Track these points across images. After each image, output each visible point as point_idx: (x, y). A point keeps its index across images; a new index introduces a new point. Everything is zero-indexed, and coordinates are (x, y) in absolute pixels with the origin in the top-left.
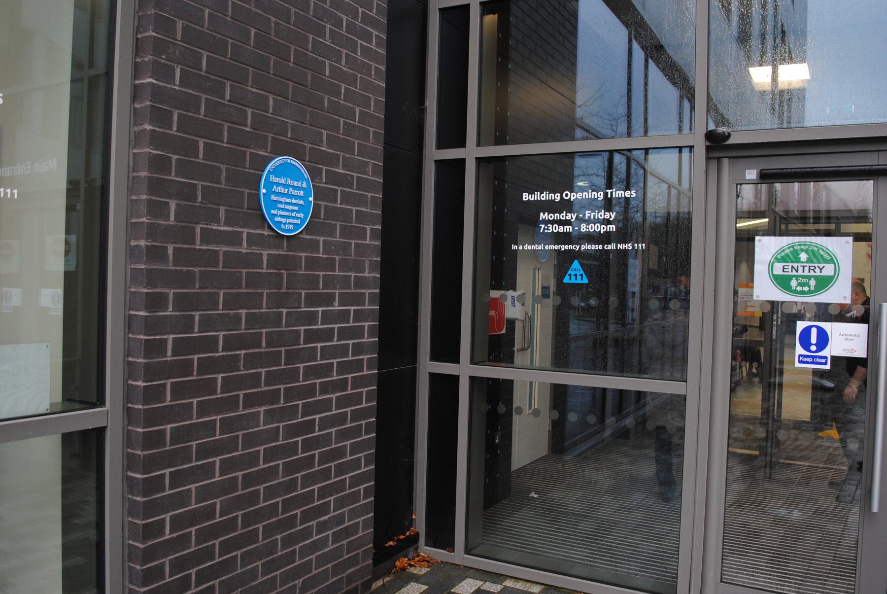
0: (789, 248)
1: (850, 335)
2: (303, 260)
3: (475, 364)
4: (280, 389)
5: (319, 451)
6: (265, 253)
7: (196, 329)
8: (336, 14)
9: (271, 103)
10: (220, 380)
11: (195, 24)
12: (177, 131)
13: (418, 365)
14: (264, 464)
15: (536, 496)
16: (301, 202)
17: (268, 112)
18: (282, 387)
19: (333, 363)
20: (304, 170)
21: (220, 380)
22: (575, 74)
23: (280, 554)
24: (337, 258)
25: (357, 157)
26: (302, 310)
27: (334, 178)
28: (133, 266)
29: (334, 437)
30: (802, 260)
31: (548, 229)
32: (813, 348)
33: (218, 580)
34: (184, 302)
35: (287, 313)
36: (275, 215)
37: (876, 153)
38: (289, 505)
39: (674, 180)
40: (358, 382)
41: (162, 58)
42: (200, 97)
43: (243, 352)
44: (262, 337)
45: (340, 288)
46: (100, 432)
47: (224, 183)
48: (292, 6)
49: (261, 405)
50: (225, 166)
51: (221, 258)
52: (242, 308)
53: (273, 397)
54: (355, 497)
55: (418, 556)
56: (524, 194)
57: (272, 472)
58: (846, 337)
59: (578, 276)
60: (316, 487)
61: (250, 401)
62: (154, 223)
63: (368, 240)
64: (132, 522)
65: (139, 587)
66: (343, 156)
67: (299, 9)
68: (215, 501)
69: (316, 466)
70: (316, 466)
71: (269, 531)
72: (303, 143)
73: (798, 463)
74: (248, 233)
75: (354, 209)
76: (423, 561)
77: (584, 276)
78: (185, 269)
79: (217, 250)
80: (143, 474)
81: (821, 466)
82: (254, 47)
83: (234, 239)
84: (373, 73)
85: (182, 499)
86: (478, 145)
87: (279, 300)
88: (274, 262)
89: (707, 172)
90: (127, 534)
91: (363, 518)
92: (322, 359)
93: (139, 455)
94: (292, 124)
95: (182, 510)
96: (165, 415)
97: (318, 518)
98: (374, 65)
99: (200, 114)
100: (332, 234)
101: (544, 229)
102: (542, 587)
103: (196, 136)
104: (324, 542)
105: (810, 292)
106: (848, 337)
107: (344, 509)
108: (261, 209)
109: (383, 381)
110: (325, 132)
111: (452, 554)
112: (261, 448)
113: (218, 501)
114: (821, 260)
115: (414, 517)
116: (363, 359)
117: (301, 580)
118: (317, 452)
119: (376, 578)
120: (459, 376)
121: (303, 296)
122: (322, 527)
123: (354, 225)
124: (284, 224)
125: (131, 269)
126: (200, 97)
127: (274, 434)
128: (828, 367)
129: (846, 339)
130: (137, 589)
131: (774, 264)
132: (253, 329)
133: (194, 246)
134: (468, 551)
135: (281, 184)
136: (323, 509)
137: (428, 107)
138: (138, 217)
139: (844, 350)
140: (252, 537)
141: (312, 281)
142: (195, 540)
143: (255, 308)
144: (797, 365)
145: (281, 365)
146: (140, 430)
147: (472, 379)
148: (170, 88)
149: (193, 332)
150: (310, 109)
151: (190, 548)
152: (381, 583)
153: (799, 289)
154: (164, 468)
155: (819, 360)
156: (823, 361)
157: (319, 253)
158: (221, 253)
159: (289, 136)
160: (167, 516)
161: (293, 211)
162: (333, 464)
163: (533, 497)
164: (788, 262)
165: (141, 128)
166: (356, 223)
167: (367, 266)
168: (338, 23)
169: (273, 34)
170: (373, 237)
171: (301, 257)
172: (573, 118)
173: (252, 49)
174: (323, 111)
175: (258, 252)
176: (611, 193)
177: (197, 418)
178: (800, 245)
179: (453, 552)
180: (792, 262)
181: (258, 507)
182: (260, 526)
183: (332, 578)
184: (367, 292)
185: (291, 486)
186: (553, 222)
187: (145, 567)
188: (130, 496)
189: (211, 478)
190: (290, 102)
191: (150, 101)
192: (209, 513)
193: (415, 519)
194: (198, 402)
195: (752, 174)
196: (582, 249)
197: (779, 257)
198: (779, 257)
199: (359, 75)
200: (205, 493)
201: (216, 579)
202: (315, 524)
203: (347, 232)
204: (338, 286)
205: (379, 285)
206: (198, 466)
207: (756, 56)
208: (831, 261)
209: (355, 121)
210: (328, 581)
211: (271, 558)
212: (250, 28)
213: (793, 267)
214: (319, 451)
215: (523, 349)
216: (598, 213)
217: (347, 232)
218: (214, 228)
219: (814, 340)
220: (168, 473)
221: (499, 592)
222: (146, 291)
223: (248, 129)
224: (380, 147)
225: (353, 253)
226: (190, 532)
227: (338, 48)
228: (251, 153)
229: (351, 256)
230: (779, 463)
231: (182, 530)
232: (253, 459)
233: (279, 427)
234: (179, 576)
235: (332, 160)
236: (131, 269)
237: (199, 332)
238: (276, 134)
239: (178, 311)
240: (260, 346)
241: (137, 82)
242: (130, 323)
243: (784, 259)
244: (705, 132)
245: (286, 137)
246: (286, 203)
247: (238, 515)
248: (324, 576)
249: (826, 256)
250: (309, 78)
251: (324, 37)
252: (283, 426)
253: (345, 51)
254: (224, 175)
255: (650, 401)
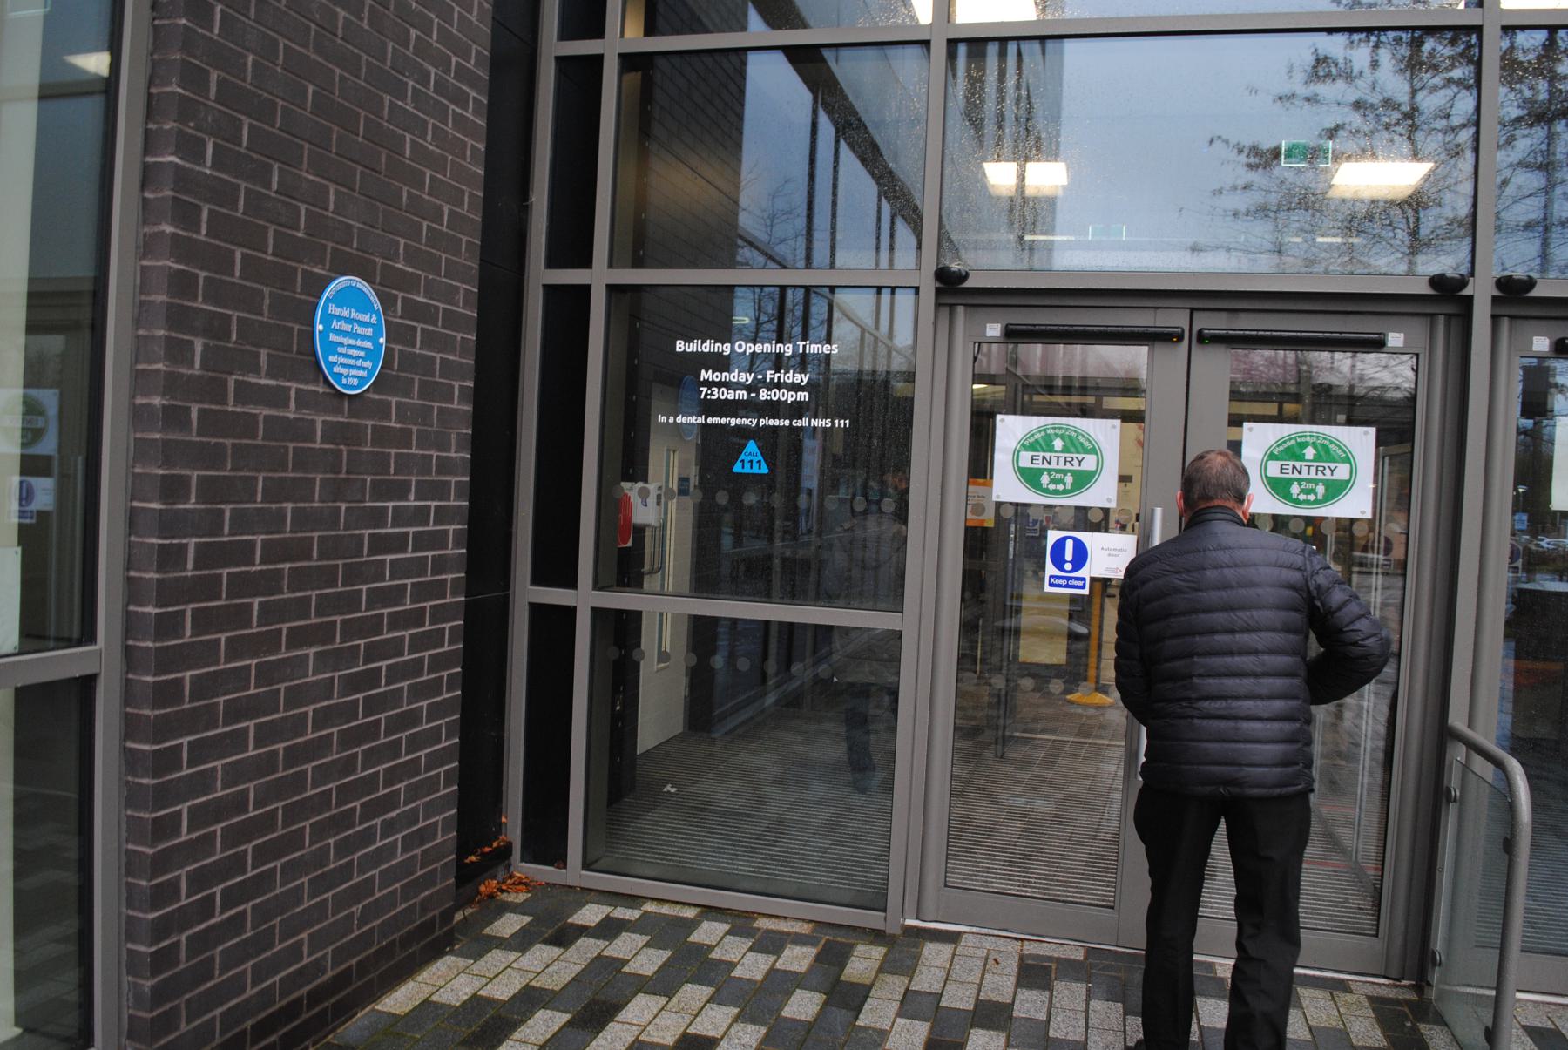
0: (1040, 432)
1: (1115, 550)
2: (369, 432)
3: (600, 589)
4: (336, 621)
5: (386, 714)
6: (319, 420)
7: (227, 529)
8: (422, 65)
9: (332, 198)
10: (256, 607)
11: (234, 76)
12: (206, 235)
13: (511, 591)
14: (312, 732)
15: (673, 790)
16: (369, 345)
17: (327, 210)
18: (338, 618)
19: (406, 585)
20: (373, 297)
21: (256, 607)
22: (740, 161)
23: (332, 866)
24: (415, 429)
25: (444, 280)
26: (367, 504)
27: (412, 310)
28: (138, 435)
29: (405, 695)
30: (1056, 448)
31: (711, 394)
32: (1068, 566)
33: (251, 904)
34: (213, 491)
35: (347, 508)
36: (335, 364)
37: (1152, 311)
38: (346, 793)
39: (869, 322)
40: (439, 614)
41: (190, 127)
42: (238, 186)
43: (287, 566)
44: (312, 545)
45: (417, 475)
46: (87, 684)
47: (266, 313)
48: (364, 52)
49: (311, 645)
50: (269, 289)
51: (261, 426)
52: (287, 500)
53: (325, 633)
54: (432, 784)
55: (511, 877)
56: (678, 342)
57: (322, 745)
58: (1108, 552)
59: (754, 462)
60: (381, 768)
61: (299, 638)
62: (174, 372)
63: (456, 402)
64: (133, 817)
65: (146, 912)
66: (426, 278)
67: (373, 57)
68: (247, 785)
69: (382, 736)
70: (382, 736)
71: (320, 831)
72: (372, 257)
73: (1039, 736)
74: (297, 389)
75: (438, 356)
76: (520, 883)
77: (763, 463)
78: (213, 441)
79: (255, 415)
80: (154, 743)
81: (1072, 739)
82: (311, 113)
83: (277, 398)
84: (468, 153)
85: (203, 783)
86: (611, 266)
87: (336, 490)
88: (332, 432)
89: (935, 324)
90: (124, 835)
91: (443, 816)
92: (392, 578)
93: (148, 717)
94: (358, 228)
95: (204, 799)
96: (184, 658)
97: (384, 814)
98: (470, 142)
99: (237, 210)
100: (408, 394)
101: (706, 394)
102: (698, 909)
103: (232, 243)
104: (390, 851)
105: (1065, 492)
106: (1113, 552)
107: (418, 803)
108: (315, 354)
109: (472, 611)
110: (402, 242)
111: (564, 871)
112: (310, 709)
113: (251, 786)
114: (1080, 450)
115: (503, 819)
116: (446, 580)
117: (360, 906)
118: (383, 716)
119: (456, 909)
120: (575, 608)
121: (368, 484)
122: (389, 827)
123: (437, 379)
124: (347, 377)
125: (135, 439)
126: (238, 186)
127: (326, 689)
128: (1086, 592)
129: (1109, 555)
130: (141, 915)
131: (1021, 454)
132: (301, 531)
133: (225, 408)
134: (587, 865)
135: (345, 318)
136: (390, 802)
137: (534, 207)
138: (150, 363)
139: (1107, 569)
140: (295, 841)
141: (381, 463)
142: (221, 843)
143: (305, 502)
144: (1047, 589)
145: (337, 586)
146: (149, 679)
147: (597, 613)
148: (199, 172)
149: (223, 535)
150: (384, 206)
151: (214, 854)
152: (462, 916)
153: (1052, 487)
154: (181, 736)
155: (1075, 583)
156: (1081, 583)
157: (390, 421)
158: (261, 419)
159: (355, 245)
160: (184, 807)
161: (357, 358)
162: (403, 735)
163: (669, 792)
164: (1038, 451)
165: (156, 229)
166: (440, 377)
167: (453, 442)
168: (424, 79)
169: (337, 93)
170: (462, 399)
171: (367, 426)
172: (734, 225)
173: (309, 115)
174: (400, 210)
175: (310, 417)
176: (804, 346)
177: (226, 663)
178: (1055, 428)
179: (565, 867)
180: (1044, 451)
181: (304, 796)
182: (307, 824)
183: (401, 904)
184: (453, 479)
185: (348, 766)
186: (720, 385)
187: (154, 882)
188: (130, 778)
189: (242, 752)
190: (356, 195)
191: (173, 190)
192: (239, 803)
193: (506, 824)
194: (228, 639)
195: (994, 330)
196: (761, 425)
197: (1027, 443)
198: (1027, 443)
199: (450, 157)
200: (235, 774)
201: (248, 901)
202: (279, 866)
203: (428, 391)
204: (415, 471)
205: (469, 471)
206: (226, 733)
207: (989, 142)
208: (1093, 451)
209: (442, 226)
210: (396, 907)
211: (320, 872)
212: (307, 83)
213: (1044, 458)
214: (386, 714)
215: (652, 572)
216: (785, 374)
217: (428, 391)
218: (253, 380)
219: (1069, 555)
220: (186, 744)
221: (637, 920)
222: (161, 472)
223: (300, 235)
224: (475, 265)
225: (435, 421)
226: (215, 832)
227: (422, 115)
228: (304, 271)
229: (432, 426)
230: (1013, 737)
231: (203, 828)
232: (298, 725)
233: (332, 679)
234: (200, 896)
235: (409, 283)
236: (135, 439)
237: (231, 534)
238: (337, 243)
239: (203, 503)
240: (309, 558)
241: (150, 159)
242: (133, 520)
243: (1032, 447)
244: (935, 269)
245: (352, 248)
246: (350, 346)
247: (277, 808)
248: (390, 902)
249: (1086, 444)
250: (383, 160)
251: (404, 99)
252: (339, 677)
253: (432, 121)
254: (267, 302)
255: (839, 647)
